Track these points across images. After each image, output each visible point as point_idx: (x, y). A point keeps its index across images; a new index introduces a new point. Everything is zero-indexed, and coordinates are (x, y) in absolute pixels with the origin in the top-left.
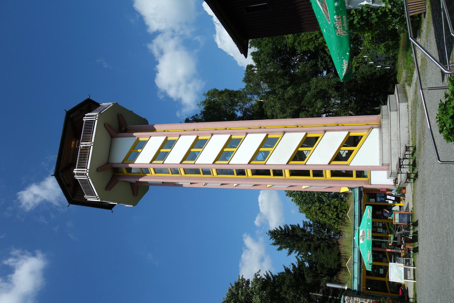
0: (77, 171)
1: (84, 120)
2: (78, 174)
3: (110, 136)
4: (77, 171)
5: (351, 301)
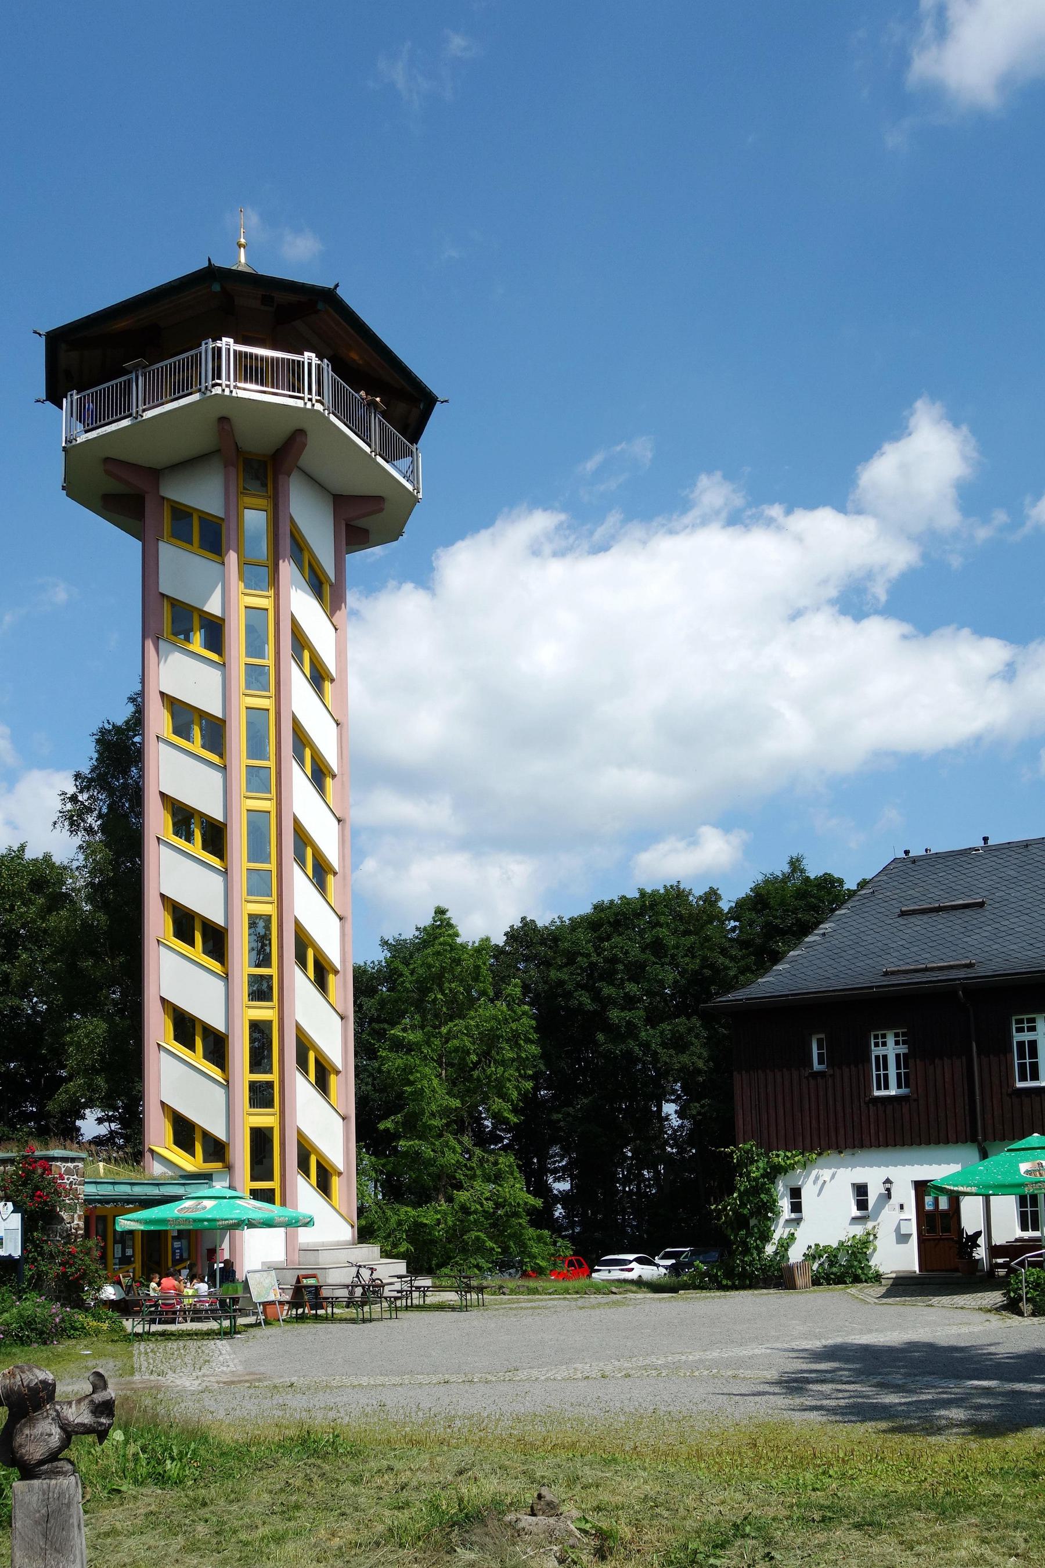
0: (310, 364)
1: (307, 354)
2: (217, 352)
3: (278, 450)
4: (310, 364)
5: (75, 1177)
